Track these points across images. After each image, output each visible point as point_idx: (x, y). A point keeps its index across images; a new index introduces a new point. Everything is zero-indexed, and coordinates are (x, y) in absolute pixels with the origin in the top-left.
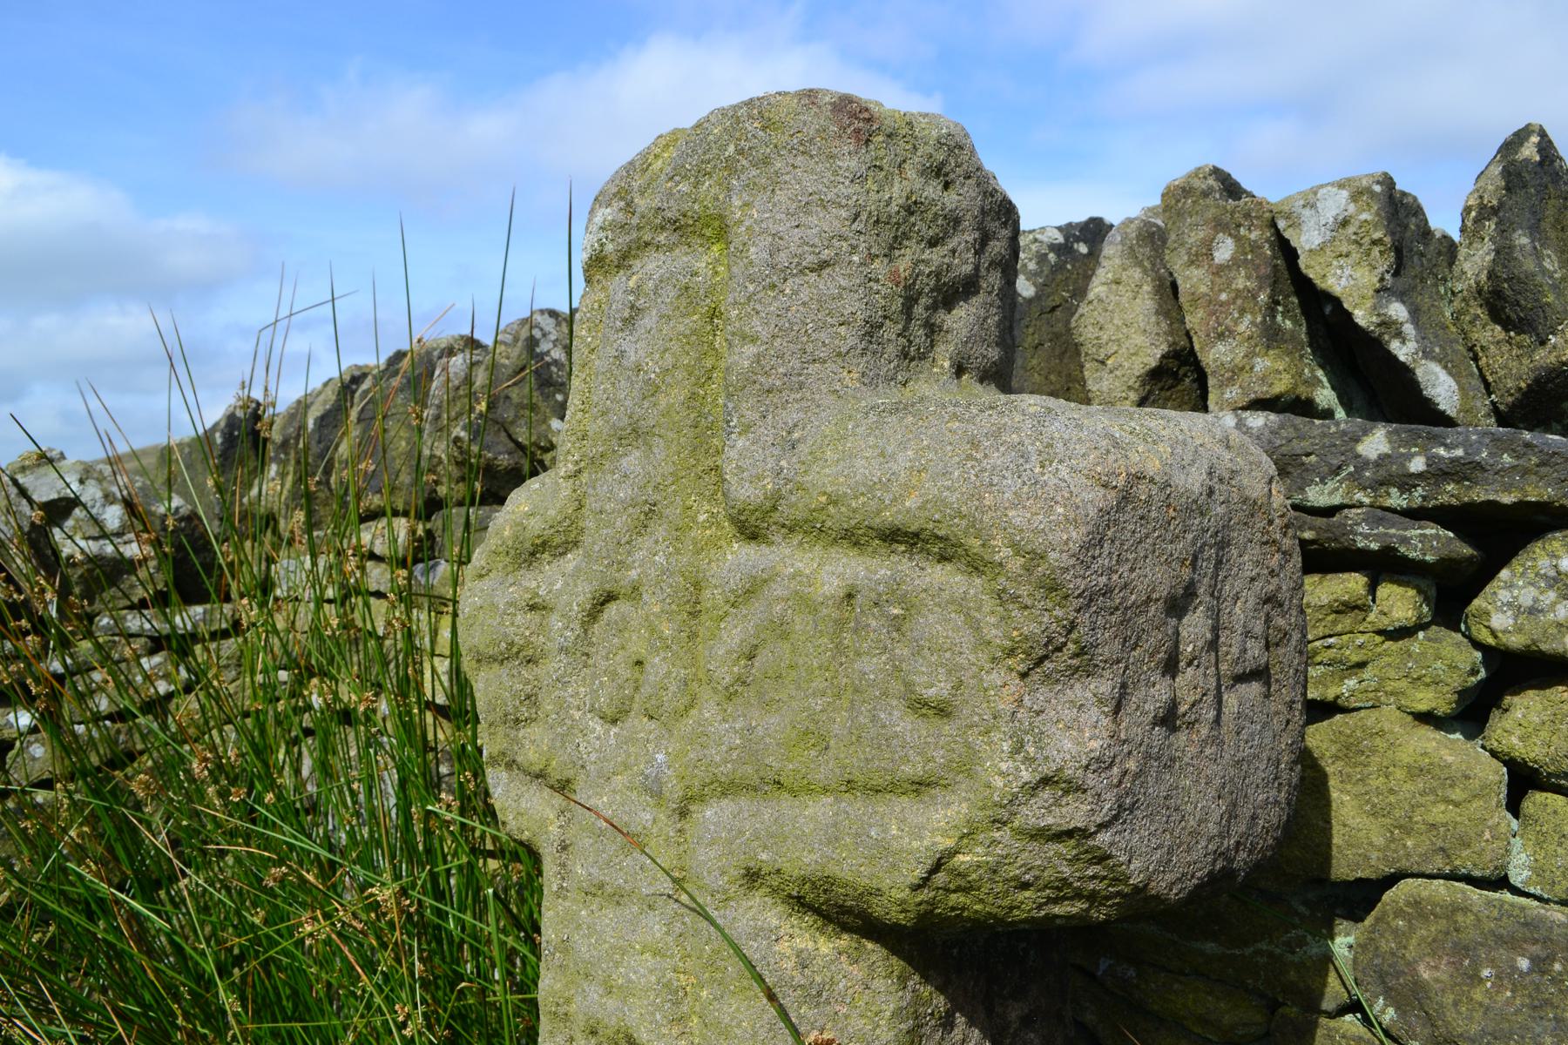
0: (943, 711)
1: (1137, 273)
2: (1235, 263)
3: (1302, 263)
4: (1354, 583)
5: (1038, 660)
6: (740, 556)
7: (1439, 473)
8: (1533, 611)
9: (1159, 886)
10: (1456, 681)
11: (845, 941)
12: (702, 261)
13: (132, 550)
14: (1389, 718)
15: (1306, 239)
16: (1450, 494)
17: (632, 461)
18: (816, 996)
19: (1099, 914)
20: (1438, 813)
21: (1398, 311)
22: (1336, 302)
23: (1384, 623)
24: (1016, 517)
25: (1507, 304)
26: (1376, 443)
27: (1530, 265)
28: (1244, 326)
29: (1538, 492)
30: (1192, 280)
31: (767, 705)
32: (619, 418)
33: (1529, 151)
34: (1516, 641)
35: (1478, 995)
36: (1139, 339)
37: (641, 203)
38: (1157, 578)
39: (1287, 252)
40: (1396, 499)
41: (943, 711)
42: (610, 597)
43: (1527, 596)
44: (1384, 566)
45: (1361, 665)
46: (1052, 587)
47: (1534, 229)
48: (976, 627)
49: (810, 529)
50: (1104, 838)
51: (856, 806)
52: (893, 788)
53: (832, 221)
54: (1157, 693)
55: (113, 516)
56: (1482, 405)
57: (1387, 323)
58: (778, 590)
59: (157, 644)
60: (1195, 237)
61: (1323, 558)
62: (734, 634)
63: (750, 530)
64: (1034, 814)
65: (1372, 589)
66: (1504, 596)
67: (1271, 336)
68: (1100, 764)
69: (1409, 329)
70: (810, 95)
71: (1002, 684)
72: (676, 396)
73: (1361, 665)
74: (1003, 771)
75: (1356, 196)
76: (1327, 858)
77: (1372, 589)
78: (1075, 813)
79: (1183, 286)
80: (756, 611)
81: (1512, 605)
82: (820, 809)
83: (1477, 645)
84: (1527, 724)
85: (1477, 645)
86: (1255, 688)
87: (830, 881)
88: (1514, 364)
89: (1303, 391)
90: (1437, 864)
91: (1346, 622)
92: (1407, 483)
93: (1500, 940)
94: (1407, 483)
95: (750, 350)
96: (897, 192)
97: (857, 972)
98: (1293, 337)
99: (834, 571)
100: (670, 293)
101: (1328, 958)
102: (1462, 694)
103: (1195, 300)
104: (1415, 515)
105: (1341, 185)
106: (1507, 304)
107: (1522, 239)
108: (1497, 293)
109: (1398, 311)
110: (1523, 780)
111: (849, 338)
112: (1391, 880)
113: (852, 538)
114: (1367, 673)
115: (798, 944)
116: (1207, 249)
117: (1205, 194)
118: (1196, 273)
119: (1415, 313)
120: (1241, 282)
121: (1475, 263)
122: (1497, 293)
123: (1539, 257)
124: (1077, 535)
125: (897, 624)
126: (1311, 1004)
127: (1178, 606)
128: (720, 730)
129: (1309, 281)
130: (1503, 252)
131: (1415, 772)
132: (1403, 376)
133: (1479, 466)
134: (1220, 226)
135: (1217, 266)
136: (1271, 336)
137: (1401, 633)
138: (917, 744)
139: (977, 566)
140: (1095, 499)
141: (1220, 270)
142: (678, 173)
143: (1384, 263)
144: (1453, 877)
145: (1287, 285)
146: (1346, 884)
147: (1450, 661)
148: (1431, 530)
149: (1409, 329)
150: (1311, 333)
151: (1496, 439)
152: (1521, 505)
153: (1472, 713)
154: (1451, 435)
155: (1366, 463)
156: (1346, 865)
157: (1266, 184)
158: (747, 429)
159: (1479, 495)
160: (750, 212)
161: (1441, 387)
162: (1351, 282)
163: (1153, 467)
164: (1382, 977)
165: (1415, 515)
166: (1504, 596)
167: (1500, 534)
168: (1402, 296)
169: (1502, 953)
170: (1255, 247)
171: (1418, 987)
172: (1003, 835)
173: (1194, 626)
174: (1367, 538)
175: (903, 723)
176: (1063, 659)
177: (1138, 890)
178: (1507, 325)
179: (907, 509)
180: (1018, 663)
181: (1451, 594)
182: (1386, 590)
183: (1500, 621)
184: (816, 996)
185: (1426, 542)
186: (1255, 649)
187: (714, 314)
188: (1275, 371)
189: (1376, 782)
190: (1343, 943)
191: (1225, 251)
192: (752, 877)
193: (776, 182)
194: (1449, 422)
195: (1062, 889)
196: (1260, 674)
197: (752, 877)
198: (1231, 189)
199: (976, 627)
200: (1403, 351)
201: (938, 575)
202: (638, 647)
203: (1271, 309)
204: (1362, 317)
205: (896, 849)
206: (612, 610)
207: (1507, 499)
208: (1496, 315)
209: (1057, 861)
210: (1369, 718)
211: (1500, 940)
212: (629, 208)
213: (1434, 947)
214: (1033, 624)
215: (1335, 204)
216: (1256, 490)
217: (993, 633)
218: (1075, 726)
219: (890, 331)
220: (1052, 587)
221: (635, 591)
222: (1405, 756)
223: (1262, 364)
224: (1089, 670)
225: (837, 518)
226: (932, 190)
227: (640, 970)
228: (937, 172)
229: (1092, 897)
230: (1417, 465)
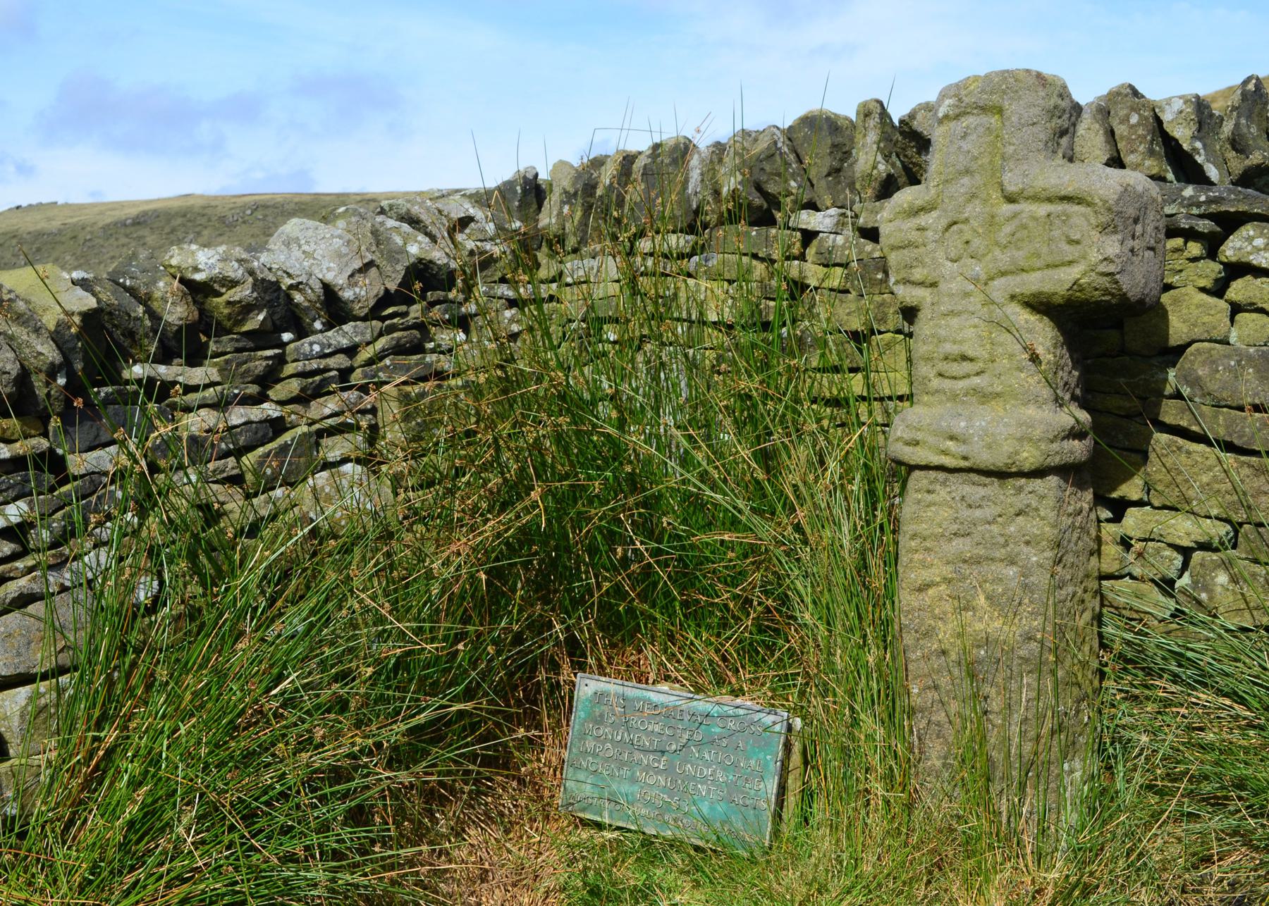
0: (1078, 242)
1: (1097, 126)
2: (1139, 124)
3: (1165, 125)
4: (1179, 241)
5: (1104, 229)
6: (1007, 208)
7: (1210, 201)
8: (1240, 249)
9: (1130, 295)
10: (1213, 276)
11: (1038, 317)
12: (994, 120)
13: (496, 251)
14: (1190, 289)
15: (1167, 117)
16: (1213, 208)
17: (966, 180)
18: (1030, 331)
19: (1114, 301)
20: (1206, 319)
21: (1198, 145)
22: (1176, 141)
23: (1190, 256)
24: (1101, 192)
25: (1238, 144)
26: (1189, 191)
27: (1245, 130)
28: (1141, 148)
29: (1243, 208)
30: (1120, 130)
31: (1019, 249)
32: (960, 167)
33: (1251, 87)
34: (1234, 259)
35: (1218, 376)
36: (1098, 152)
37: (966, 100)
38: (1131, 212)
39: (1159, 121)
40: (1195, 211)
41: (1078, 242)
42: (955, 223)
43: (1238, 244)
44: (1190, 235)
45: (1181, 271)
46: (1109, 209)
47: (1249, 118)
48: (1088, 221)
49: (1035, 198)
50: (1118, 277)
51: (1050, 272)
52: (1063, 264)
53: (1036, 111)
54: (1130, 243)
55: (490, 228)
56: (1227, 180)
57: (1194, 149)
58: (1024, 215)
59: (512, 303)
60: (1123, 113)
61: (1172, 232)
62: (1008, 229)
63: (1011, 199)
64: (1103, 268)
65: (1185, 243)
66: (1231, 245)
67: (1151, 153)
68: (1118, 256)
69: (1202, 151)
70: (1028, 71)
71: (1095, 234)
72: (986, 160)
73: (1181, 271)
74: (1094, 257)
75: (1185, 102)
76: (1167, 339)
77: (1185, 243)
78: (1112, 268)
79: (1117, 132)
80: (1016, 222)
81: (1233, 248)
82: (1038, 274)
83: (1221, 263)
84: (1239, 289)
85: (1221, 263)
86: (1152, 253)
87: (1041, 293)
88: (1238, 165)
89: (1162, 174)
90: (1205, 336)
91: (1176, 255)
92: (1199, 205)
93: (1225, 356)
94: (1199, 205)
95: (1012, 148)
96: (1052, 102)
97: (1041, 325)
98: (1159, 153)
99: (1042, 209)
100: (981, 130)
101: (1166, 380)
102: (1216, 280)
103: (1122, 138)
104: (1201, 216)
105: (1180, 97)
106: (1238, 144)
107: (1243, 121)
108: (1234, 140)
109: (1198, 145)
110: (1236, 309)
111: (1041, 145)
112: (1189, 344)
113: (1049, 200)
114: (1183, 274)
115: (1024, 317)
116: (1127, 118)
117: (1126, 95)
118: (1123, 127)
119: (1205, 146)
120: (1140, 132)
121: (1228, 128)
122: (1234, 140)
123: (1249, 127)
124: (1116, 197)
125: (1064, 221)
126: (1160, 395)
127: (1136, 221)
128: (1003, 259)
129: (1167, 133)
130: (1237, 125)
131: (1198, 306)
132: (1199, 169)
133: (1223, 199)
134: (1133, 109)
135: (1130, 125)
136: (1151, 153)
137: (1195, 260)
138: (1070, 252)
139: (1089, 204)
140: (1120, 189)
141: (1132, 126)
142: (983, 91)
143: (1194, 128)
144: (1210, 341)
145: (1158, 133)
146: (1173, 347)
147: (1212, 269)
148: (1207, 222)
149: (1202, 151)
150: (1166, 152)
151: (1229, 189)
152: (1237, 212)
153: (1218, 290)
154: (1214, 188)
155: (1185, 199)
156: (1174, 341)
157: (1152, 91)
158: (1011, 171)
159: (1223, 208)
160: (1011, 107)
161: (1212, 172)
162: (1182, 134)
163: (1132, 183)
164: (1185, 377)
165: (1201, 216)
166: (1231, 245)
167: (1230, 223)
168: (1200, 139)
169: (1226, 361)
170: (1146, 118)
171: (1198, 379)
172: (1093, 274)
173: (1139, 228)
174: (1184, 224)
175: (1066, 247)
176: (1110, 229)
177: (1125, 294)
178: (1237, 151)
179: (1069, 190)
180: (1100, 229)
181: (1212, 246)
182: (1190, 244)
183: (1229, 253)
184: (1030, 331)
185: (1205, 226)
186: (1152, 241)
187: (997, 136)
188: (1153, 165)
189: (1185, 311)
190: (1172, 374)
191: (1134, 119)
192: (1013, 297)
193: (1020, 98)
194: (1212, 184)
195: (1106, 292)
196: (1152, 249)
197: (1013, 297)
198: (1135, 93)
199: (1088, 221)
200: (1199, 159)
201: (1076, 208)
202: (967, 236)
203: (1152, 143)
204: (1185, 147)
205: (1058, 282)
206: (955, 227)
207: (1232, 210)
208: (1234, 148)
209: (1104, 282)
210: (1183, 290)
211: (1225, 356)
212: (960, 100)
213: (1204, 363)
214: (1104, 219)
215: (1178, 105)
216: (1155, 195)
217: (1093, 221)
218: (1112, 246)
219: (1050, 144)
220: (1109, 209)
221: (967, 221)
222: (1195, 301)
223: (1147, 163)
224: (1115, 232)
225: (1044, 194)
226: (1060, 102)
227: (970, 333)
228: (1061, 96)
229: (1113, 295)
230: (1203, 198)
